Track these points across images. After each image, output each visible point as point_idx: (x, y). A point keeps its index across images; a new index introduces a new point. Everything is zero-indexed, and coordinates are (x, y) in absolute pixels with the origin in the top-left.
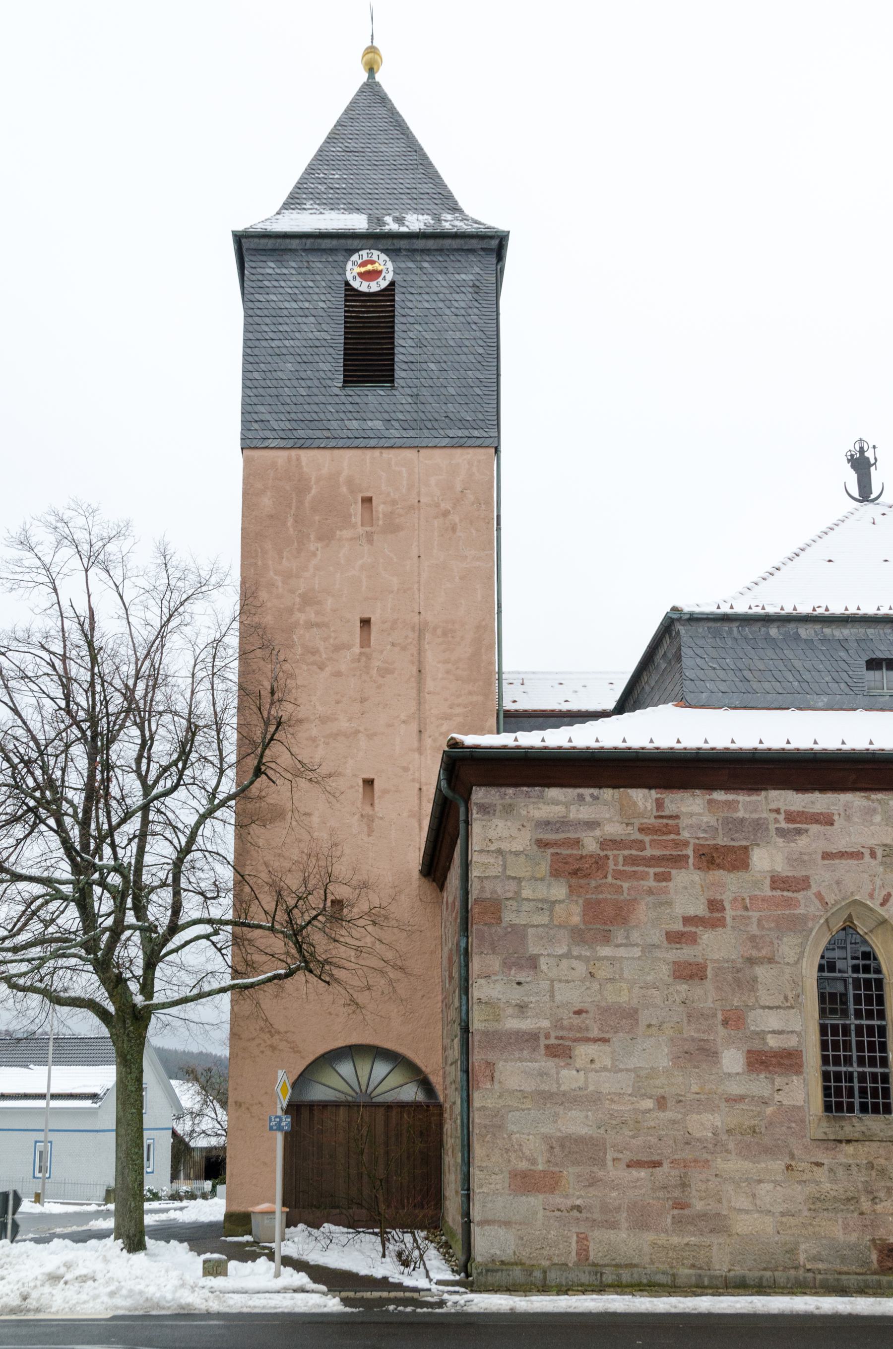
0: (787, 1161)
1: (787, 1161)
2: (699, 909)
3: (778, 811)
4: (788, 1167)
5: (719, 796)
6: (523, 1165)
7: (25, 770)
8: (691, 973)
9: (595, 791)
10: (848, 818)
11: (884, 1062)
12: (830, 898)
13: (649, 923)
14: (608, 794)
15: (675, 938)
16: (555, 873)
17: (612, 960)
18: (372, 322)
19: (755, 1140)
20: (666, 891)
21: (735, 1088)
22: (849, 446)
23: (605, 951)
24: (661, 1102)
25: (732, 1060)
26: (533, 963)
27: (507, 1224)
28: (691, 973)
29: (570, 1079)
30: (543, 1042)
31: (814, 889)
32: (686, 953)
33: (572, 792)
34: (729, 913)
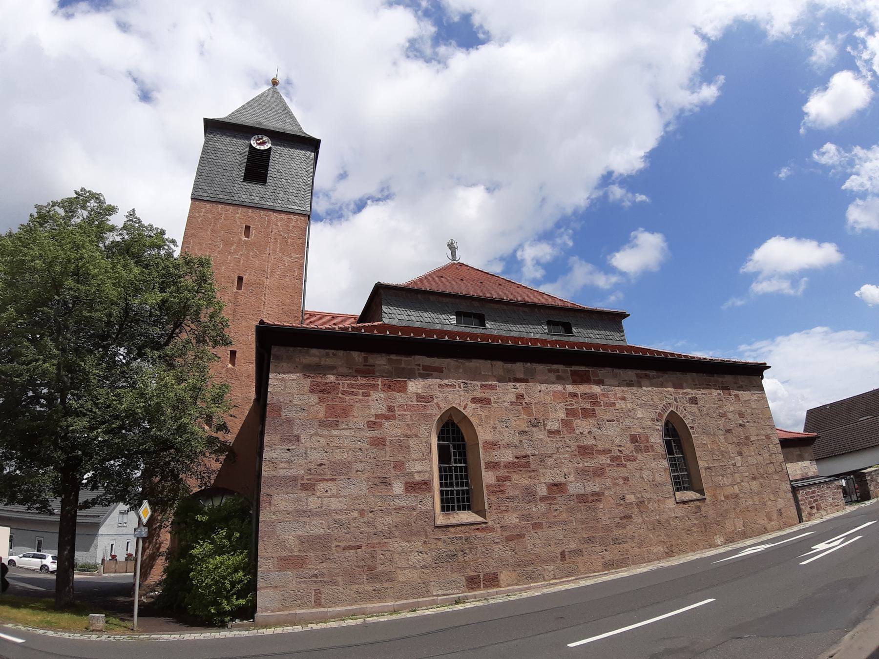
0: (424, 539)
1: (424, 539)
2: (383, 410)
3: (419, 365)
5: (394, 357)
6: (285, 553)
7: (756, 498)
8: (379, 443)
9: (334, 351)
10: (449, 370)
11: (467, 485)
12: (442, 405)
13: (359, 418)
14: (341, 353)
15: (372, 425)
16: (312, 391)
17: (339, 437)
19: (407, 531)
20: (367, 401)
21: (399, 503)
22: (448, 241)
23: (335, 432)
24: (362, 513)
25: (398, 488)
26: (297, 438)
27: (275, 587)
28: (379, 443)
29: (313, 503)
31: (436, 401)
32: (376, 433)
33: (323, 351)
34: (397, 413)
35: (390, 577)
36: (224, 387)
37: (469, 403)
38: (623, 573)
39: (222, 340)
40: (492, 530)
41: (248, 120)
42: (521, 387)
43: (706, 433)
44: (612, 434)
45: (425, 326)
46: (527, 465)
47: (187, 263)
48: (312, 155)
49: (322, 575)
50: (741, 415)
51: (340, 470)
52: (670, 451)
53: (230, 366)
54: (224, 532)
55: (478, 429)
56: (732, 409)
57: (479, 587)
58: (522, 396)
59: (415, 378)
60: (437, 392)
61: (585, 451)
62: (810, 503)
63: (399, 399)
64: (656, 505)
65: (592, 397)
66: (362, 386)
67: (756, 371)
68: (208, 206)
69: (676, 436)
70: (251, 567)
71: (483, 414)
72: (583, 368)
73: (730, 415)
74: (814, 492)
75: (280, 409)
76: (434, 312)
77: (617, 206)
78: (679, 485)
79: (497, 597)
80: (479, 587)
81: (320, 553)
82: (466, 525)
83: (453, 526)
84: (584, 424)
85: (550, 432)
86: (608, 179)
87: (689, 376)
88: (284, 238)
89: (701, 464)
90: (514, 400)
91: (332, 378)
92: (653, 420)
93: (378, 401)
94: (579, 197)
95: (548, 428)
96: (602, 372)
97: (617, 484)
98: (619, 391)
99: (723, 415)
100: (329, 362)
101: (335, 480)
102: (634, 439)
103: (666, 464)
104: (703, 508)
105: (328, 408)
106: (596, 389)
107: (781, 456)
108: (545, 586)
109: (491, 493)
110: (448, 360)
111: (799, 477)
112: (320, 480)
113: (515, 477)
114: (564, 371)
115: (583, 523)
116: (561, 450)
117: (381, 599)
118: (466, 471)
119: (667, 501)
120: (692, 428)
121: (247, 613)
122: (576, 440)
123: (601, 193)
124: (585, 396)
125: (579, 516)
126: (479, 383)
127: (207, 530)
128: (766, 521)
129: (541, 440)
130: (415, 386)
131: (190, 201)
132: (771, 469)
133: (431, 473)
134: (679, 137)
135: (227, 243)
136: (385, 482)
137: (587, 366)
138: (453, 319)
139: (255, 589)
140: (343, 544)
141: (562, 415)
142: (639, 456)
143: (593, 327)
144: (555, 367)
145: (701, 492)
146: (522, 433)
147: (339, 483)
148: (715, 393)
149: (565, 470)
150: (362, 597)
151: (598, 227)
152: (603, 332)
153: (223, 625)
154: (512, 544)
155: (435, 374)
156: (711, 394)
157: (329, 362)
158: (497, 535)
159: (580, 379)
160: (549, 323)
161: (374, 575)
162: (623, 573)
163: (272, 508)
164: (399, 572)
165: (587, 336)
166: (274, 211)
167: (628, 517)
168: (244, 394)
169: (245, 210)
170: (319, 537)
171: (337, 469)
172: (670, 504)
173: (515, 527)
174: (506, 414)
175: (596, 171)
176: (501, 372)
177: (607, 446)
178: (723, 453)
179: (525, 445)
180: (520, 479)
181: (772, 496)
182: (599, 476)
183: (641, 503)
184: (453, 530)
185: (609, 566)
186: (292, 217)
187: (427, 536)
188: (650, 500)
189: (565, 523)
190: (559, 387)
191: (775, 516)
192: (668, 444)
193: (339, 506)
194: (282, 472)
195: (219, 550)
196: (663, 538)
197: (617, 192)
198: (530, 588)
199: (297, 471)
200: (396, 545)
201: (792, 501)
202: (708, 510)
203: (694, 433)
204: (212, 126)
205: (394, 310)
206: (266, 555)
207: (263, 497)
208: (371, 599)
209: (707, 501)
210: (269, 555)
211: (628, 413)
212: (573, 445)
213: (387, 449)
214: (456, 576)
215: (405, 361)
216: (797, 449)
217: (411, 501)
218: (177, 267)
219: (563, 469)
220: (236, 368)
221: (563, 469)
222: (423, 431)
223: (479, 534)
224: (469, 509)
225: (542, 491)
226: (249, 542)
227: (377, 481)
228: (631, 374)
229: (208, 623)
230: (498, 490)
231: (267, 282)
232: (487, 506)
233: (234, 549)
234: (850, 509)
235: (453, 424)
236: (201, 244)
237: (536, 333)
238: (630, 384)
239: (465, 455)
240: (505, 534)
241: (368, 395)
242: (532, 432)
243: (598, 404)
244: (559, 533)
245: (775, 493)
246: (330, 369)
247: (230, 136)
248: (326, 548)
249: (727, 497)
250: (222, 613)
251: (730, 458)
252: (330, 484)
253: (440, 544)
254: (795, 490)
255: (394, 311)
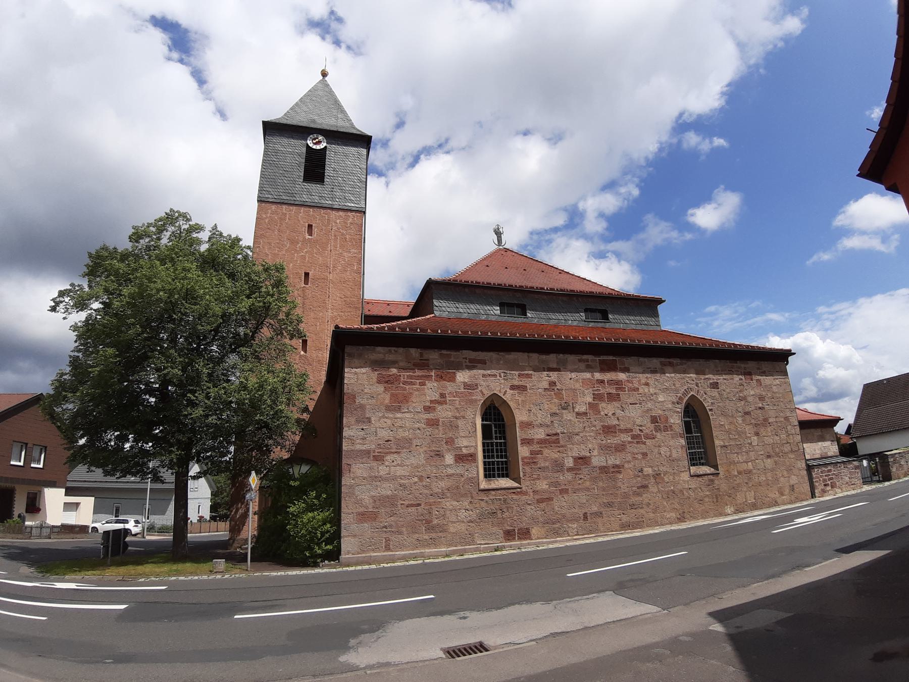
1: (470, 499)
2: (436, 397)
4: (471, 502)
5: (444, 352)
6: (362, 510)
11: (506, 457)
12: (485, 392)
13: (417, 404)
14: (401, 350)
15: (427, 409)
16: (379, 382)
17: (401, 419)
18: (387, 184)
19: (456, 493)
21: (450, 471)
23: (399, 415)
24: (421, 478)
25: (449, 459)
26: (369, 420)
27: (355, 536)
29: (383, 471)
30: (372, 454)
32: (430, 416)
33: (387, 349)
34: (448, 398)
35: (443, 529)
36: (304, 375)
37: (508, 390)
38: (637, 533)
39: (297, 334)
40: (525, 493)
41: (301, 119)
42: (554, 376)
43: (724, 414)
44: (634, 415)
45: (471, 316)
46: (557, 441)
47: (266, 270)
48: (364, 151)
49: (391, 526)
50: (762, 398)
51: (403, 445)
52: (688, 429)
53: (302, 353)
54: (314, 494)
55: (516, 412)
56: (752, 393)
57: (514, 539)
58: (555, 383)
59: (463, 369)
60: (482, 382)
61: (609, 430)
62: (825, 480)
63: (450, 387)
64: (671, 478)
65: (618, 383)
66: (419, 377)
67: (783, 356)
68: (274, 207)
69: (695, 418)
70: (336, 521)
71: (520, 399)
72: (611, 358)
73: (750, 399)
74: (830, 471)
75: (354, 397)
76: (480, 304)
77: (694, 154)
78: (694, 460)
79: (528, 547)
80: (514, 539)
81: (388, 510)
82: (505, 489)
83: (493, 490)
84: (609, 406)
85: (578, 414)
86: (682, 126)
87: (711, 363)
88: (343, 234)
89: (717, 443)
90: (547, 387)
91: (394, 371)
92: (673, 403)
93: (432, 389)
94: (648, 144)
95: (576, 410)
96: (628, 361)
97: (637, 459)
98: (643, 377)
99: (743, 399)
100: (391, 357)
101: (399, 453)
102: (654, 420)
103: (683, 442)
104: (716, 482)
105: (392, 395)
106: (622, 376)
107: (799, 437)
108: (569, 540)
109: (525, 464)
110: (491, 353)
111: (817, 456)
112: (387, 453)
113: (546, 452)
114: (593, 361)
115: (604, 490)
116: (587, 429)
117: (436, 546)
118: (505, 446)
119: (682, 474)
120: (711, 410)
121: (334, 555)
122: (601, 421)
123: (675, 140)
124: (611, 382)
125: (601, 484)
126: (517, 373)
127: (301, 492)
128: (777, 495)
129: (570, 420)
130: (462, 376)
131: (256, 204)
132: (787, 448)
133: (476, 447)
134: (762, 71)
135: (293, 242)
136: (439, 455)
137: (614, 355)
138: (497, 310)
139: (339, 537)
140: (406, 503)
141: (589, 399)
142: (658, 435)
143: (628, 314)
144: (585, 357)
145: (716, 467)
146: (553, 414)
147: (402, 455)
148: (737, 378)
149: (590, 446)
150: (421, 543)
151: (667, 180)
152: (638, 318)
153: (315, 565)
154: (543, 505)
155: (479, 365)
156: (732, 379)
157: (391, 357)
158: (530, 498)
159: (607, 367)
160: (586, 311)
161: (430, 526)
162: (637, 533)
163: (352, 475)
164: (450, 524)
165: (624, 325)
166: (332, 209)
167: (645, 487)
168: (318, 377)
169: (307, 209)
170: (388, 497)
171: (403, 440)
172: (685, 477)
173: (544, 491)
174: (538, 399)
175: (669, 112)
176: (537, 363)
177: (629, 426)
178: (739, 433)
179: (556, 425)
180: (550, 453)
181: (785, 473)
182: (619, 451)
183: (657, 475)
184: (493, 493)
185: (625, 527)
186: (349, 214)
187: (472, 498)
188: (666, 473)
189: (588, 489)
190: (588, 375)
191: (787, 491)
192: (687, 425)
193: (403, 473)
194: (358, 447)
195: (310, 508)
196: (677, 506)
197: (692, 139)
198: (556, 542)
199: (370, 446)
200: (448, 504)
201: (806, 478)
202: (721, 483)
203: (712, 415)
204: (271, 129)
205: (444, 304)
206: (348, 511)
207: (344, 466)
208: (428, 546)
209: (721, 475)
210: (350, 511)
211: (650, 397)
212: (599, 425)
213: (441, 428)
214: (495, 529)
215: (454, 356)
216: (819, 430)
217: (459, 470)
218: (258, 274)
219: (589, 445)
220: (308, 354)
221: (589, 445)
222: (469, 413)
223: (515, 497)
224: (507, 476)
225: (569, 462)
226: (334, 502)
227: (432, 454)
228: (655, 362)
229: (304, 564)
230: (531, 461)
231: (331, 277)
232: (521, 474)
233: (322, 508)
234: (866, 488)
235: (495, 408)
236: (270, 244)
237: (572, 324)
238: (654, 371)
239: (504, 432)
240: (537, 497)
241: (424, 385)
242: (562, 414)
243: (622, 389)
244: (583, 497)
245: (789, 470)
246: (393, 363)
247: (288, 138)
248: (394, 505)
249: (740, 473)
250: (315, 556)
251: (747, 438)
252: (395, 456)
253: (483, 504)
254: (809, 468)
255: (444, 305)
